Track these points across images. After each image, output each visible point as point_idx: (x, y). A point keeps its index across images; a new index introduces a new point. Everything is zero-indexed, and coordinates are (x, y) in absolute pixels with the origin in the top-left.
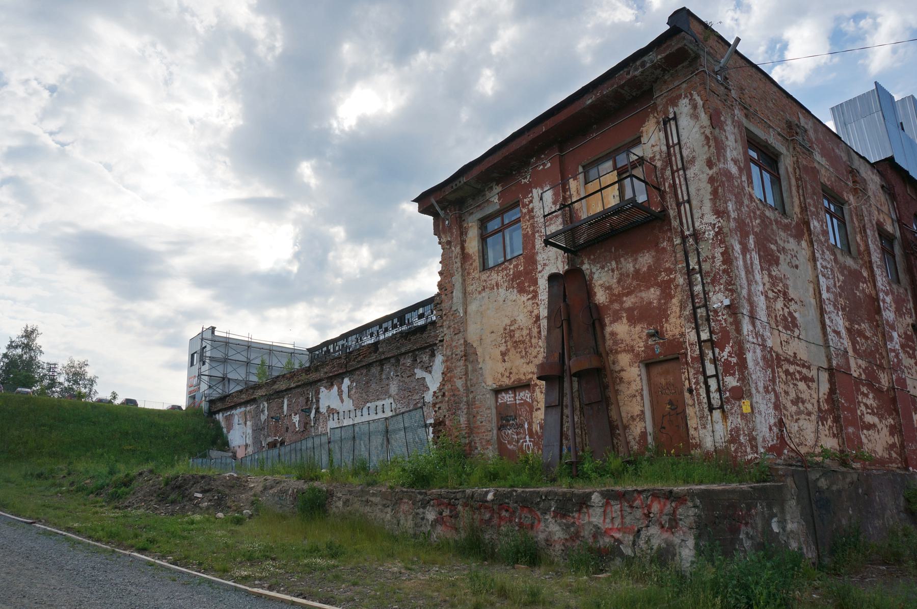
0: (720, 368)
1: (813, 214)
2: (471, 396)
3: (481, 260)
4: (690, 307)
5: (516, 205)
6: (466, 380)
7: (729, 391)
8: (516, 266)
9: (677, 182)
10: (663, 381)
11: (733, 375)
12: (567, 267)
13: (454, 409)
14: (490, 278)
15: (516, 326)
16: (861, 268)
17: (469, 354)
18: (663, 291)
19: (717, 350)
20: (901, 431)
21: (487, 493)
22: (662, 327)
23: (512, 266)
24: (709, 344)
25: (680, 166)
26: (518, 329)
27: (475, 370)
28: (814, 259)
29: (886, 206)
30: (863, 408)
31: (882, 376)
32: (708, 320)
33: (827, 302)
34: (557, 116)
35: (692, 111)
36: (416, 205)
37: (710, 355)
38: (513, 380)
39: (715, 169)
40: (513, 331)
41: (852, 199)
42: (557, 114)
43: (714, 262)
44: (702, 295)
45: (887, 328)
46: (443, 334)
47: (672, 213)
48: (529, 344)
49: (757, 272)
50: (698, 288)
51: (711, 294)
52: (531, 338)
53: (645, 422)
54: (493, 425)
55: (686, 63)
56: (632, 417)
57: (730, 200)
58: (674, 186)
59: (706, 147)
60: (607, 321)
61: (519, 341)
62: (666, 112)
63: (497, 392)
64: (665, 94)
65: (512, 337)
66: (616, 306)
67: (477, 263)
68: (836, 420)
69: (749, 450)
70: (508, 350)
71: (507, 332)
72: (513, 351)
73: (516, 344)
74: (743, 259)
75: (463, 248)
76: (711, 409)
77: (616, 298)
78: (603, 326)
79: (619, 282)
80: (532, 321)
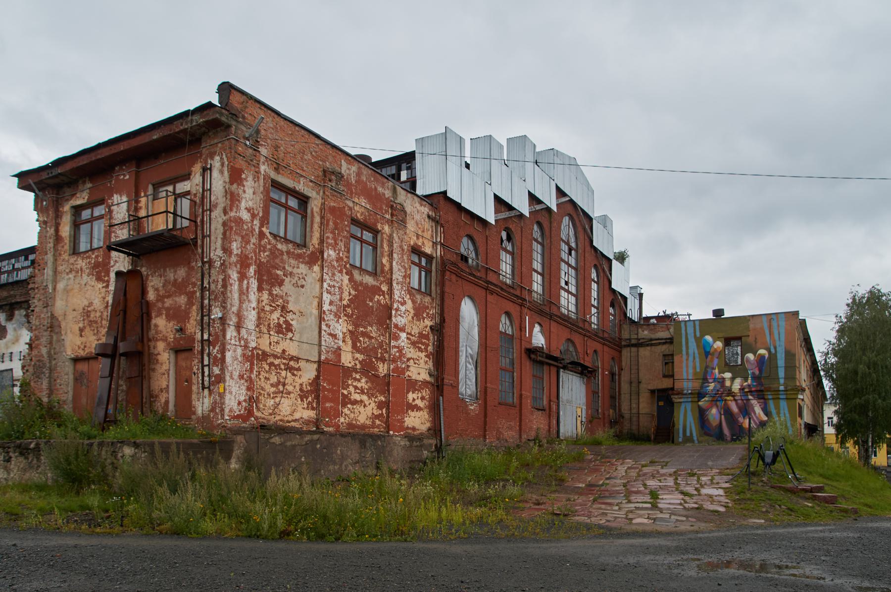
0: (211, 363)
1: (329, 245)
2: (54, 362)
3: (72, 244)
4: (200, 315)
5: (101, 202)
6: (50, 349)
7: (215, 377)
8: (97, 257)
9: (205, 219)
10: (184, 364)
11: (217, 366)
12: (130, 268)
13: (37, 374)
14: (77, 262)
15: (92, 308)
16: (381, 284)
17: (54, 326)
18: (189, 299)
19: (211, 348)
20: (388, 406)
21: (31, 443)
22: (185, 325)
23: (94, 256)
24: (207, 343)
25: (208, 208)
26: (94, 310)
27: (58, 341)
28: (322, 280)
29: (430, 232)
30: (352, 389)
31: (381, 366)
32: (209, 326)
33: (327, 313)
34: (133, 140)
35: (220, 167)
36: (16, 180)
37: (207, 351)
38: (86, 352)
39: (227, 217)
40: (89, 312)
41: (387, 228)
42: (133, 138)
43: (217, 285)
44: (207, 307)
45: (394, 330)
46: (34, 306)
47: (199, 242)
48: (100, 325)
49: (252, 293)
50: (206, 302)
51: (213, 307)
52: (102, 320)
53: (168, 394)
54: (69, 389)
55: (222, 128)
56: (161, 389)
57: (236, 241)
58: (202, 221)
59: (225, 198)
60: (153, 315)
61: (94, 321)
62: (206, 163)
63: (76, 360)
64: (208, 147)
65: (88, 316)
66: (160, 305)
67: (67, 246)
68: (317, 397)
69: (220, 417)
70: (85, 327)
71: (85, 311)
72: (88, 329)
73: (91, 323)
74: (239, 284)
75: (57, 231)
76: (203, 388)
77: (160, 299)
78: (149, 318)
79: (163, 286)
80: (104, 306)
